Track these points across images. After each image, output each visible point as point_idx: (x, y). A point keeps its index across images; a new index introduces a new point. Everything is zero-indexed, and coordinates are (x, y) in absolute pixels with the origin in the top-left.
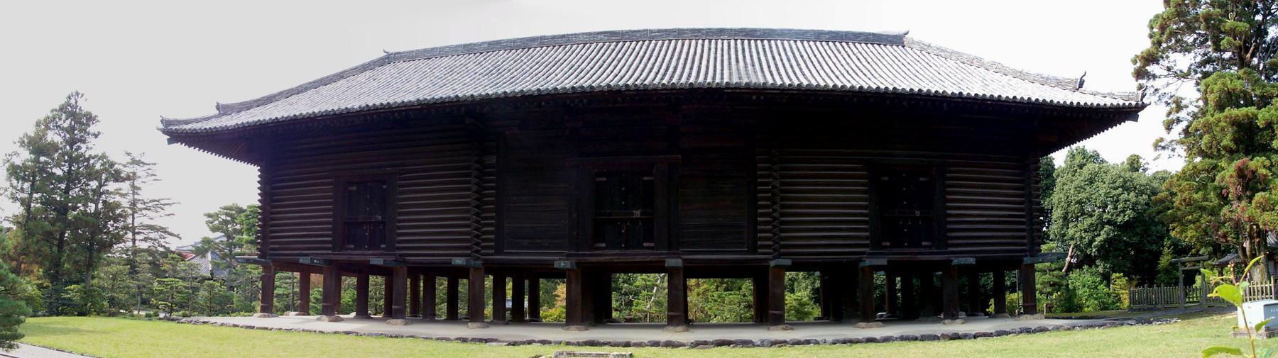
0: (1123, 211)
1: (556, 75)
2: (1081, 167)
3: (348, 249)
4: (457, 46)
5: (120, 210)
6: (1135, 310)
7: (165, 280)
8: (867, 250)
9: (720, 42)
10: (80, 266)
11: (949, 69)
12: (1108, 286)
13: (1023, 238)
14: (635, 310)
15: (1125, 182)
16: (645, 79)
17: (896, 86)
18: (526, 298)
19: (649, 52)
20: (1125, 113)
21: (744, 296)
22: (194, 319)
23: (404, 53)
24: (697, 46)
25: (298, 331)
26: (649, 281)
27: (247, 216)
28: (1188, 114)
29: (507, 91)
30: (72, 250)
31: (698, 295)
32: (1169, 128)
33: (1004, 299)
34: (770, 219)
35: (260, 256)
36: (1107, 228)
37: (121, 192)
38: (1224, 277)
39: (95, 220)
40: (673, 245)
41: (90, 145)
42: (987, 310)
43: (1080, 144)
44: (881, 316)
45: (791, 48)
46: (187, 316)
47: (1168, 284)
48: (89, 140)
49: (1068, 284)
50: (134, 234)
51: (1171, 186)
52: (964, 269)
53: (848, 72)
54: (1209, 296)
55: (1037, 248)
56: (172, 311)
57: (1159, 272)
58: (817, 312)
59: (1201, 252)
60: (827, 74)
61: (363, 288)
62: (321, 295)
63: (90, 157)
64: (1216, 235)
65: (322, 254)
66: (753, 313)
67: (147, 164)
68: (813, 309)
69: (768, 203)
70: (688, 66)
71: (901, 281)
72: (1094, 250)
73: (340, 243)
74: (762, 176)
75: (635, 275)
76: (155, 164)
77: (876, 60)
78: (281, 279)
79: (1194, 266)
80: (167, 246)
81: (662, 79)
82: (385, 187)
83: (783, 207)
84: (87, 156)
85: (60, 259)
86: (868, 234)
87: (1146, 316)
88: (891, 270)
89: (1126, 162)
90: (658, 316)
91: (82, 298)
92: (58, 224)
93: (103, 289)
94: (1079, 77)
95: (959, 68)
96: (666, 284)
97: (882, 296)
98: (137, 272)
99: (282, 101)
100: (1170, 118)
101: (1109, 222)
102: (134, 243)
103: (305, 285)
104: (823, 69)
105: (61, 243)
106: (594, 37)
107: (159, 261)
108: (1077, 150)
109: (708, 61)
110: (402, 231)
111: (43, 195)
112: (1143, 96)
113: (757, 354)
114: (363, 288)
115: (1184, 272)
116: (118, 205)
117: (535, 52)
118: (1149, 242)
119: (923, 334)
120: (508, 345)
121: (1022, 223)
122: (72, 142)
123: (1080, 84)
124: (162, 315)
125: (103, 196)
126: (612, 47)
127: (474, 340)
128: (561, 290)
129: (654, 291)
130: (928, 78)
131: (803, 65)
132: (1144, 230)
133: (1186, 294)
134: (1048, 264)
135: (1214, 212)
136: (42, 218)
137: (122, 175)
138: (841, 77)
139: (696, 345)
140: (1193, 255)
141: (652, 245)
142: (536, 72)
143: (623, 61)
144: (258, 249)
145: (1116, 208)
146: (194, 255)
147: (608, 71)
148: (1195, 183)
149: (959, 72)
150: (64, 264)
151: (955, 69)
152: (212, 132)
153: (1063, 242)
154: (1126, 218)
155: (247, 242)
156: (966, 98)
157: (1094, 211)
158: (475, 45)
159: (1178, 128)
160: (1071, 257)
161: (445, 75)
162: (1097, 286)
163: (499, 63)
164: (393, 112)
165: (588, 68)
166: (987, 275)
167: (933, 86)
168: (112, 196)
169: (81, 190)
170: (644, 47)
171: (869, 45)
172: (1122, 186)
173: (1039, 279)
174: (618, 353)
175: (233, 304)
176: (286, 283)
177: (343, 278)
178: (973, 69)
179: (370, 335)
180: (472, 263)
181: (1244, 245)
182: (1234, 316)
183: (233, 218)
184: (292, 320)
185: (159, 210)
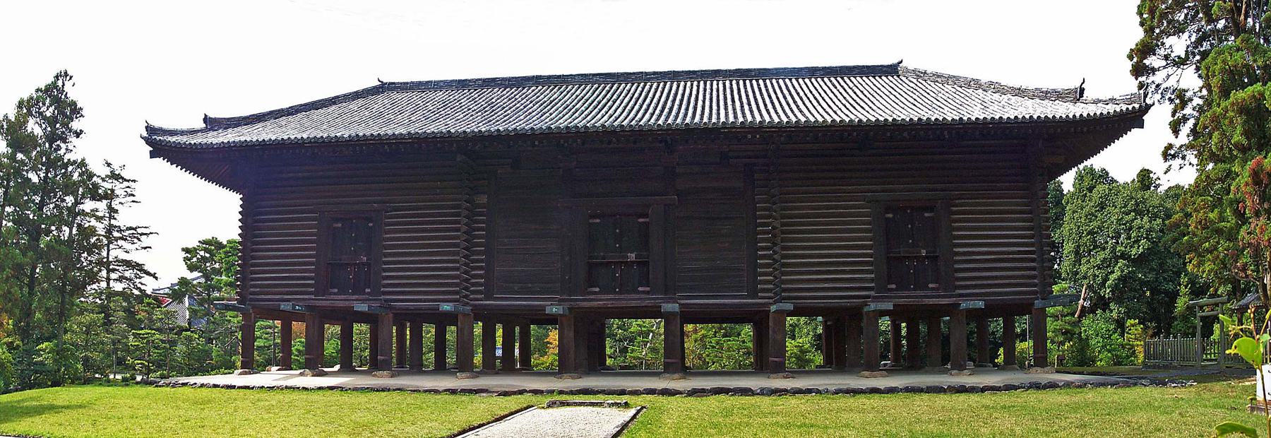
0: (1137, 241)
1: (551, 114)
2: (1090, 189)
3: (330, 294)
4: (451, 81)
5: (95, 238)
6: (1149, 367)
7: (140, 332)
8: (872, 293)
9: (715, 83)
10: (51, 314)
11: (947, 95)
12: (1122, 335)
13: (1034, 277)
14: (630, 357)
15: (1137, 204)
16: (641, 119)
17: (895, 116)
18: (517, 345)
19: (644, 94)
20: (1132, 119)
21: (744, 342)
22: (173, 380)
23: (398, 83)
24: (692, 88)
25: (280, 388)
26: (645, 327)
27: (226, 253)
28: (1193, 110)
29: (500, 128)
30: (44, 292)
31: (695, 342)
32: (1175, 130)
33: (1014, 349)
34: (772, 286)
35: (240, 302)
36: (1121, 262)
37: (97, 213)
38: (1244, 326)
39: (68, 250)
40: (669, 290)
41: (70, 147)
42: (996, 361)
43: (1088, 163)
44: (885, 365)
45: (787, 86)
46: (165, 378)
47: (1185, 335)
48: (70, 140)
49: (1081, 333)
50: (109, 271)
51: (1185, 205)
52: (973, 314)
53: (845, 106)
54: (1227, 352)
55: (1049, 289)
56: (149, 371)
57: (1175, 318)
58: (819, 359)
59: (1219, 293)
60: (824, 110)
61: (346, 337)
62: (303, 347)
63: (70, 163)
64: (1234, 268)
65: (304, 299)
66: (752, 360)
67: (126, 180)
68: (814, 356)
69: (769, 244)
70: (684, 107)
71: (907, 327)
72: (1108, 291)
73: (322, 289)
74: (762, 217)
75: (630, 321)
76: (134, 181)
77: (872, 92)
78: (262, 328)
79: (1212, 310)
80: (143, 287)
81: (658, 119)
82: (371, 225)
83: (784, 248)
84: (66, 161)
85: (31, 305)
86: (873, 276)
87: (1161, 375)
88: (896, 315)
89: (1136, 180)
90: (654, 363)
91: (55, 360)
92: (30, 254)
93: (76, 346)
94: (1078, 85)
95: (957, 93)
96: (662, 330)
97: (887, 343)
98: (111, 323)
99: (271, 121)
100: (1176, 118)
101: (1123, 256)
102: (108, 284)
103: (287, 334)
104: (820, 105)
105: (33, 282)
106: (590, 79)
107: (134, 308)
108: (1084, 170)
109: (704, 102)
110: (387, 274)
111: (15, 210)
112: (1146, 96)
113: (756, 402)
114: (346, 337)
115: (1203, 319)
116: (93, 231)
117: (530, 91)
118: (1165, 279)
119: (929, 385)
120: (498, 395)
121: (1033, 260)
122: (52, 138)
123: (1080, 94)
124: (139, 378)
125: (79, 218)
126: (607, 88)
127: (464, 391)
128: (554, 336)
129: (650, 338)
130: (927, 106)
131: (800, 103)
132: (1160, 264)
133: (1204, 349)
134: (1060, 308)
135: (1232, 236)
136: (12, 243)
137: (100, 191)
138: (839, 112)
139: (693, 393)
140: (1212, 296)
141: (648, 289)
142: (531, 111)
143: (618, 102)
144: (237, 292)
145: (1129, 238)
146: (171, 300)
147: (603, 112)
148: (1209, 198)
149: (958, 97)
150: (35, 312)
151: (953, 94)
152: (196, 148)
153: (1075, 281)
154: (1141, 250)
155: (227, 284)
156: (967, 123)
157: (1107, 242)
158: (470, 81)
159: (1186, 129)
160: (1084, 300)
161: (438, 109)
162: (1111, 335)
163: (493, 100)
164: (383, 144)
165: (583, 108)
166: (996, 321)
167: (932, 113)
168: (87, 218)
169: (56, 206)
170: (640, 89)
171: (864, 78)
172: (1134, 211)
173: (1051, 325)
174: (613, 402)
175: (212, 360)
176: (267, 332)
177: (326, 326)
178: (971, 92)
179: (356, 389)
180: (461, 308)
181: (1265, 282)
182: (1253, 383)
183: (212, 255)
184: (272, 377)
185: (136, 240)
